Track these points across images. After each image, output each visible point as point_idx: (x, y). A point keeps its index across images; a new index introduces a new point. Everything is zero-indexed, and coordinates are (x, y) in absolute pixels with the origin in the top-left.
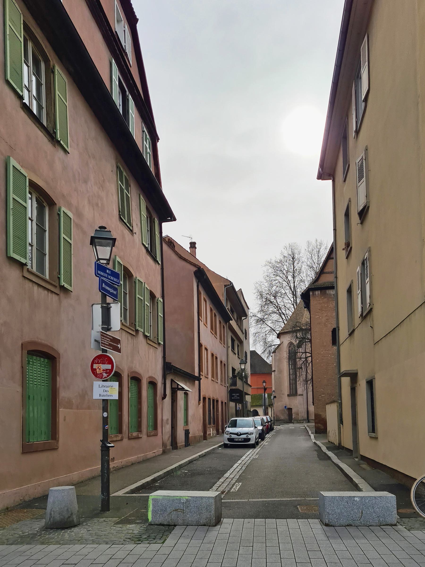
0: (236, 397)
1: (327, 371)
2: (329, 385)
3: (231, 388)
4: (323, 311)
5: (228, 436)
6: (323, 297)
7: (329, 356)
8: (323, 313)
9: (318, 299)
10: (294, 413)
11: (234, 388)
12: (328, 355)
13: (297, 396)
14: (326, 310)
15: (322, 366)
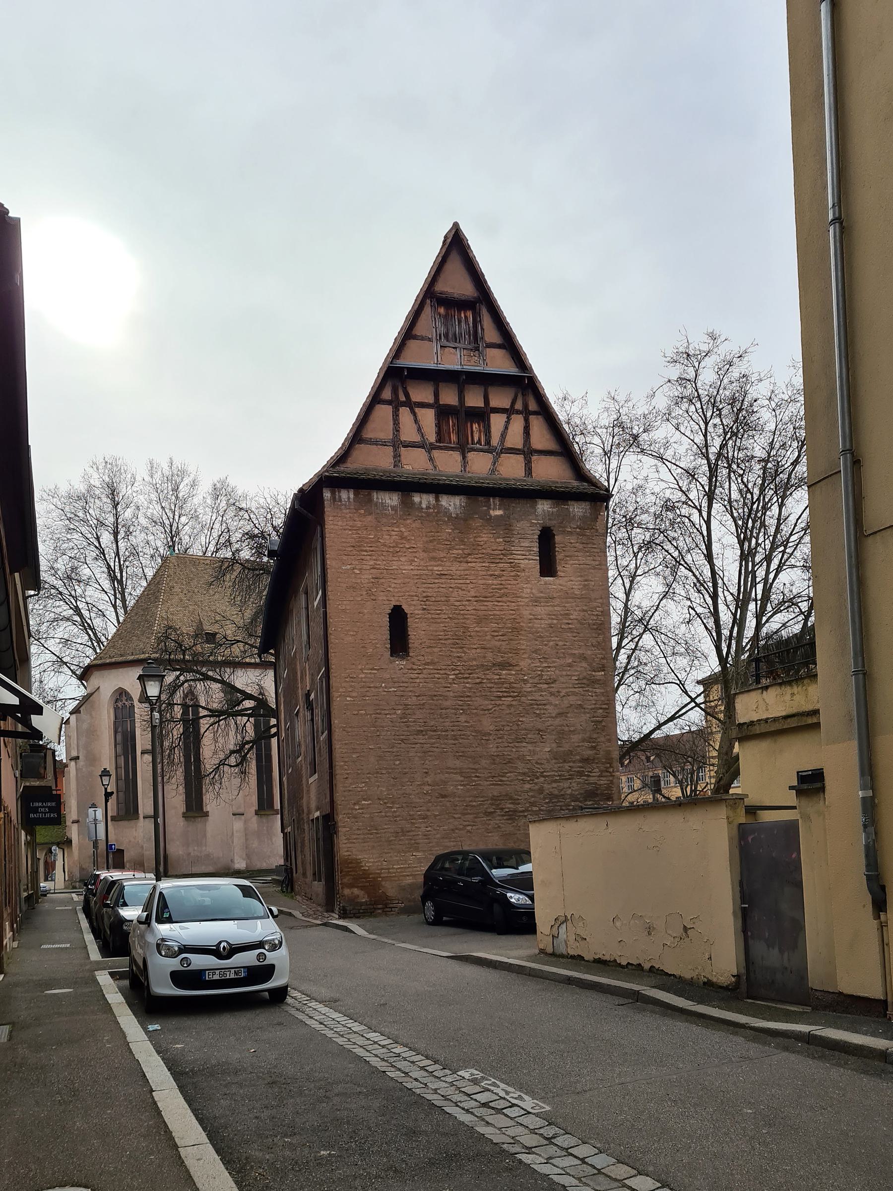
0: (45, 813)
1: (378, 731)
2: (384, 772)
3: (28, 784)
4: (362, 551)
5: (174, 964)
6: (362, 511)
7: (381, 686)
8: (363, 557)
9: (348, 516)
10: (129, 861)
11: (37, 783)
12: (378, 685)
13: (138, 818)
14: (371, 549)
15: (361, 714)
